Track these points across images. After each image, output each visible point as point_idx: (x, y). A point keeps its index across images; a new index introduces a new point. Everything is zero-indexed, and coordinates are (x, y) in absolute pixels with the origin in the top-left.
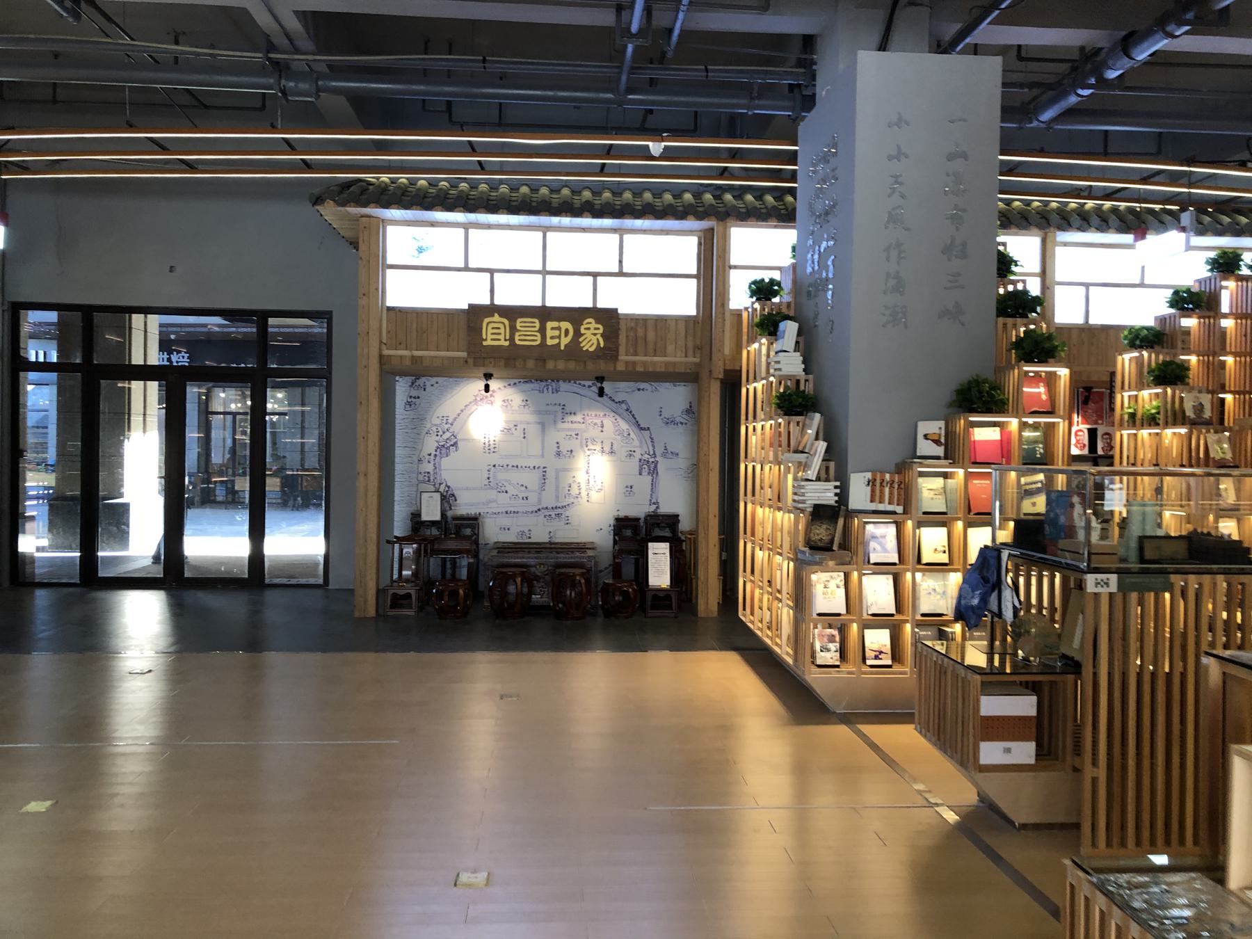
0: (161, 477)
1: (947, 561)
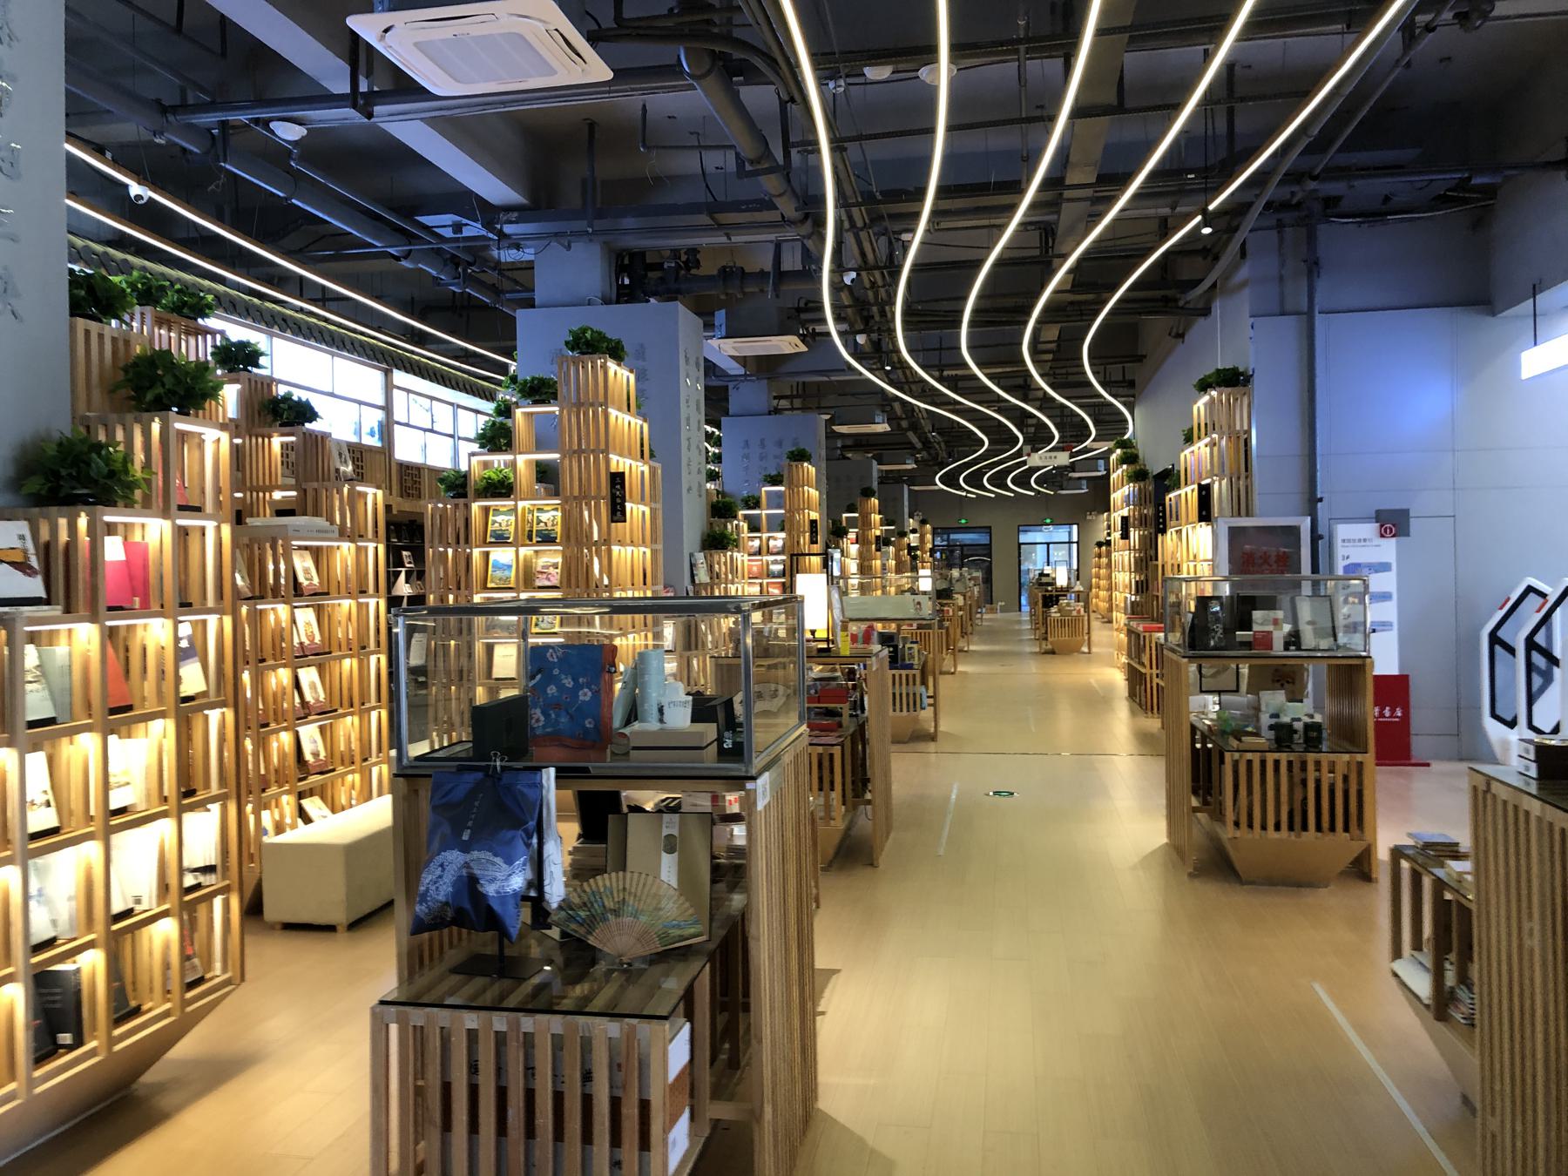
0: (823, 1013)
1: (54, 823)
